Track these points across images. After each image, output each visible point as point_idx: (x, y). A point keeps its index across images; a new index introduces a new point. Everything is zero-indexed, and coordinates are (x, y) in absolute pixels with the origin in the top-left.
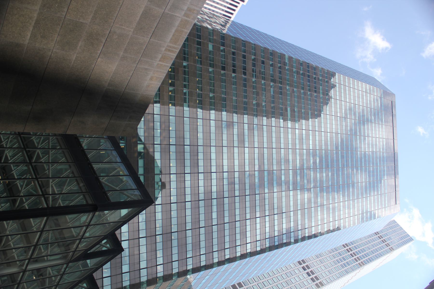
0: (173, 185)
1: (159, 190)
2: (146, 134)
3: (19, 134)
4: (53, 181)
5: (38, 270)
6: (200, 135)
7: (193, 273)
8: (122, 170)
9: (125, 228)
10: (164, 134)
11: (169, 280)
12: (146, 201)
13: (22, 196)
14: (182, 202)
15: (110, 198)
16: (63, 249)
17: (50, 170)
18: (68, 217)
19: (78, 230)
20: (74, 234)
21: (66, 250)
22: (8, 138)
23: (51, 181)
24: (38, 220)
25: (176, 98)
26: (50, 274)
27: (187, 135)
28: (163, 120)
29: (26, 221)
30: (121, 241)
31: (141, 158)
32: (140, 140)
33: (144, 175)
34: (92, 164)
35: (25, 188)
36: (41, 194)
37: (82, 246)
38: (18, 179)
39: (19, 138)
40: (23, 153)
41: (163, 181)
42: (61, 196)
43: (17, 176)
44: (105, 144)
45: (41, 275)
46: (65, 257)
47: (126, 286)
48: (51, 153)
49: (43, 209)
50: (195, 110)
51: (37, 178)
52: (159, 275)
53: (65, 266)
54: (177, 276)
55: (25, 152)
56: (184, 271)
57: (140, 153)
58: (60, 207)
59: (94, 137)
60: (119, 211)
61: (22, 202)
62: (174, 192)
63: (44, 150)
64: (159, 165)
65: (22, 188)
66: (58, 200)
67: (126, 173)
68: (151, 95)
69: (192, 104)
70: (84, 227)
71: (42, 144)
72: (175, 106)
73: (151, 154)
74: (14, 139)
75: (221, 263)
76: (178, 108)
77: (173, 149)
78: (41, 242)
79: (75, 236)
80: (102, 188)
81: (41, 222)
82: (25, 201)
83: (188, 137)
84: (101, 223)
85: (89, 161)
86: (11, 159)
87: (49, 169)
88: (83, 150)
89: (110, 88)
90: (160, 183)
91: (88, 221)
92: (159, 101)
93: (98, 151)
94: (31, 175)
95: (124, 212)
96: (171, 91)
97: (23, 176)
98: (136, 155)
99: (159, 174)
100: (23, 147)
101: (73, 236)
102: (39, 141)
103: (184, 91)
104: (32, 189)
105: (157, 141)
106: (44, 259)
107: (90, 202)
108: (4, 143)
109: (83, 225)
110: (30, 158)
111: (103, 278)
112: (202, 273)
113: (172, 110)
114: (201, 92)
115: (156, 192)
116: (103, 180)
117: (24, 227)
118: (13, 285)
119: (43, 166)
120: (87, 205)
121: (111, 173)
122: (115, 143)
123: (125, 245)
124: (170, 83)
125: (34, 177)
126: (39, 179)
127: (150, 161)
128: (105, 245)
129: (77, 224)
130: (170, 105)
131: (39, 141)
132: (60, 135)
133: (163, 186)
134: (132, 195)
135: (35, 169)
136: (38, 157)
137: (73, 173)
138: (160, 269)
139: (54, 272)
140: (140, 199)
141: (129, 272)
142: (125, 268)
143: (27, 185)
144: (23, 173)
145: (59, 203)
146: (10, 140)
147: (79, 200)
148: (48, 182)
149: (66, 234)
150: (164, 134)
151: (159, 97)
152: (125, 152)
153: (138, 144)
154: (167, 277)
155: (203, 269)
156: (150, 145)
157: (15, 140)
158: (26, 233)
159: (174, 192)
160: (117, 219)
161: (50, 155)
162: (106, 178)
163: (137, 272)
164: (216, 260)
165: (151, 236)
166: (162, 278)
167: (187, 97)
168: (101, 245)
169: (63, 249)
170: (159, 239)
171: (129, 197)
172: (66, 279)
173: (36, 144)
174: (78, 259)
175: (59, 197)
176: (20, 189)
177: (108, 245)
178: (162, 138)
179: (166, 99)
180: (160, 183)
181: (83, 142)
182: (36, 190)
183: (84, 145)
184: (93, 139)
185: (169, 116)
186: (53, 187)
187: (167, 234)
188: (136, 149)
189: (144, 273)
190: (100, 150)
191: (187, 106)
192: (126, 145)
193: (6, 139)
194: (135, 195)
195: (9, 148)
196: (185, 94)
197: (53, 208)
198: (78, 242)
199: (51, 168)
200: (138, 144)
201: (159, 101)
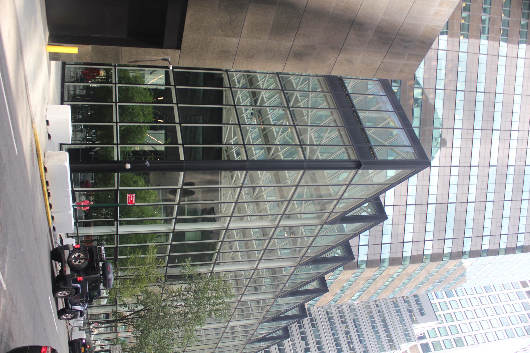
0: (457, 143)
1: (437, 149)
2: (426, 76)
3: (277, 74)
4: (312, 129)
5: (290, 227)
6: (501, 79)
7: (470, 257)
8: (394, 120)
9: (390, 193)
10: (450, 77)
11: (438, 261)
12: (421, 162)
13: (277, 145)
14: (466, 167)
15: (377, 154)
16: (318, 207)
17: (309, 116)
18: (327, 173)
19: (336, 188)
20: (332, 192)
21: (321, 210)
22: (265, 77)
23: (309, 128)
24: (292, 172)
25: (470, 28)
26: (302, 233)
27: (482, 78)
28: (450, 58)
29: (281, 172)
30: (385, 206)
31: (417, 106)
32: (418, 83)
33: (420, 128)
34: (358, 111)
35: (281, 135)
36: (298, 144)
37: (341, 207)
38: (273, 125)
39: (277, 78)
40: (280, 96)
41: (443, 137)
42: (320, 147)
43: (273, 121)
44: (374, 87)
45: (293, 233)
46: (319, 217)
47: (407, 257)
48: (311, 96)
49: (301, 161)
50: (496, 43)
51: (294, 126)
52: (405, 255)
53: (319, 227)
54: (448, 258)
55: (282, 94)
56: (458, 252)
57: (417, 100)
58: (318, 161)
59: (362, 79)
60: (385, 170)
61: (277, 150)
62: (456, 152)
63: (302, 93)
64: (441, 117)
65: (277, 135)
66: (316, 152)
67: (398, 124)
68: (440, 26)
69: (492, 35)
70: (347, 187)
71: (301, 85)
72: (468, 38)
73: (431, 101)
74: (271, 78)
75: (509, 251)
76: (472, 40)
77: (460, 96)
78: (294, 198)
79: (333, 195)
80: (368, 141)
81: (298, 174)
82: (280, 149)
83: (483, 81)
84: (363, 183)
85: (355, 108)
86: (267, 101)
87: (307, 115)
88: (348, 95)
89: (386, 18)
90: (439, 140)
91: (349, 179)
92: (447, 32)
93: (365, 96)
94: (289, 122)
95: (391, 173)
96: (463, 18)
97: (279, 121)
98: (411, 102)
99: (439, 128)
100: (280, 88)
101: (330, 195)
102: (299, 81)
103: (483, 18)
104: (288, 136)
105: (440, 85)
106: (298, 217)
107: (353, 158)
108: (260, 82)
109: (342, 183)
110: (288, 101)
111: (359, 246)
112: (482, 258)
113: (464, 44)
114: (508, 19)
115: (434, 150)
116: (370, 132)
117: (278, 180)
118: (265, 240)
119: (302, 111)
120: (350, 161)
121: (380, 124)
122: (386, 85)
123: (388, 211)
124: (464, 7)
125: (292, 124)
126: (297, 127)
127: (428, 111)
128: (367, 210)
129: (335, 182)
130: (462, 37)
131: (299, 81)
132: (322, 76)
133: (443, 143)
134: (404, 153)
135: (292, 114)
136: (297, 100)
137: (335, 121)
138: (429, 245)
139: (306, 231)
140: (414, 159)
141: (390, 243)
142: (386, 239)
143: (283, 132)
144: (278, 119)
145: (318, 155)
146: (267, 79)
147: (340, 154)
148: (307, 129)
149: (323, 191)
150: (450, 77)
151: (448, 30)
152: (398, 97)
153: (414, 87)
154: (436, 257)
155: (485, 254)
156: (431, 90)
157: (272, 80)
158: (279, 185)
159: (456, 152)
160: (382, 180)
161: (310, 98)
162: (373, 130)
163: (400, 245)
164: (503, 246)
165: (422, 204)
166: (429, 257)
167: (487, 26)
168: (362, 209)
169: (318, 207)
170: (431, 209)
171: (399, 155)
172: (318, 242)
173: (295, 86)
174: (333, 222)
175: (318, 148)
176: (276, 136)
177: (369, 210)
178: (446, 81)
179: (457, 28)
180: (440, 139)
181: (349, 83)
182: (292, 138)
183: (349, 89)
184: (360, 81)
185: (476, 92)
186: (310, 135)
187: (443, 206)
188: (411, 94)
189: (408, 247)
190: (367, 94)
191: (486, 38)
192: (400, 89)
193: (263, 78)
194: (408, 153)
195: (265, 89)
196: (484, 21)
197: (310, 161)
198: (335, 202)
199: (310, 114)
200: (414, 87)
201: (447, 32)
